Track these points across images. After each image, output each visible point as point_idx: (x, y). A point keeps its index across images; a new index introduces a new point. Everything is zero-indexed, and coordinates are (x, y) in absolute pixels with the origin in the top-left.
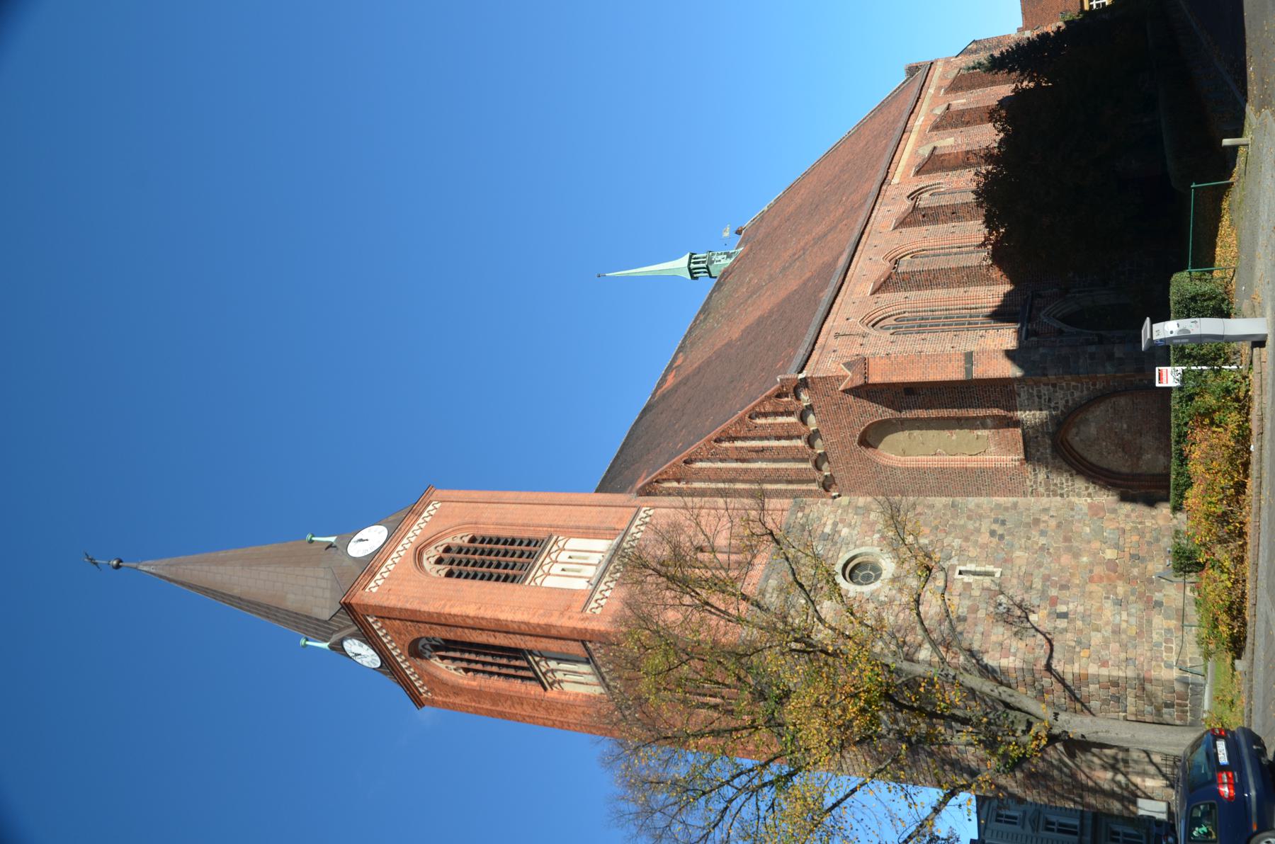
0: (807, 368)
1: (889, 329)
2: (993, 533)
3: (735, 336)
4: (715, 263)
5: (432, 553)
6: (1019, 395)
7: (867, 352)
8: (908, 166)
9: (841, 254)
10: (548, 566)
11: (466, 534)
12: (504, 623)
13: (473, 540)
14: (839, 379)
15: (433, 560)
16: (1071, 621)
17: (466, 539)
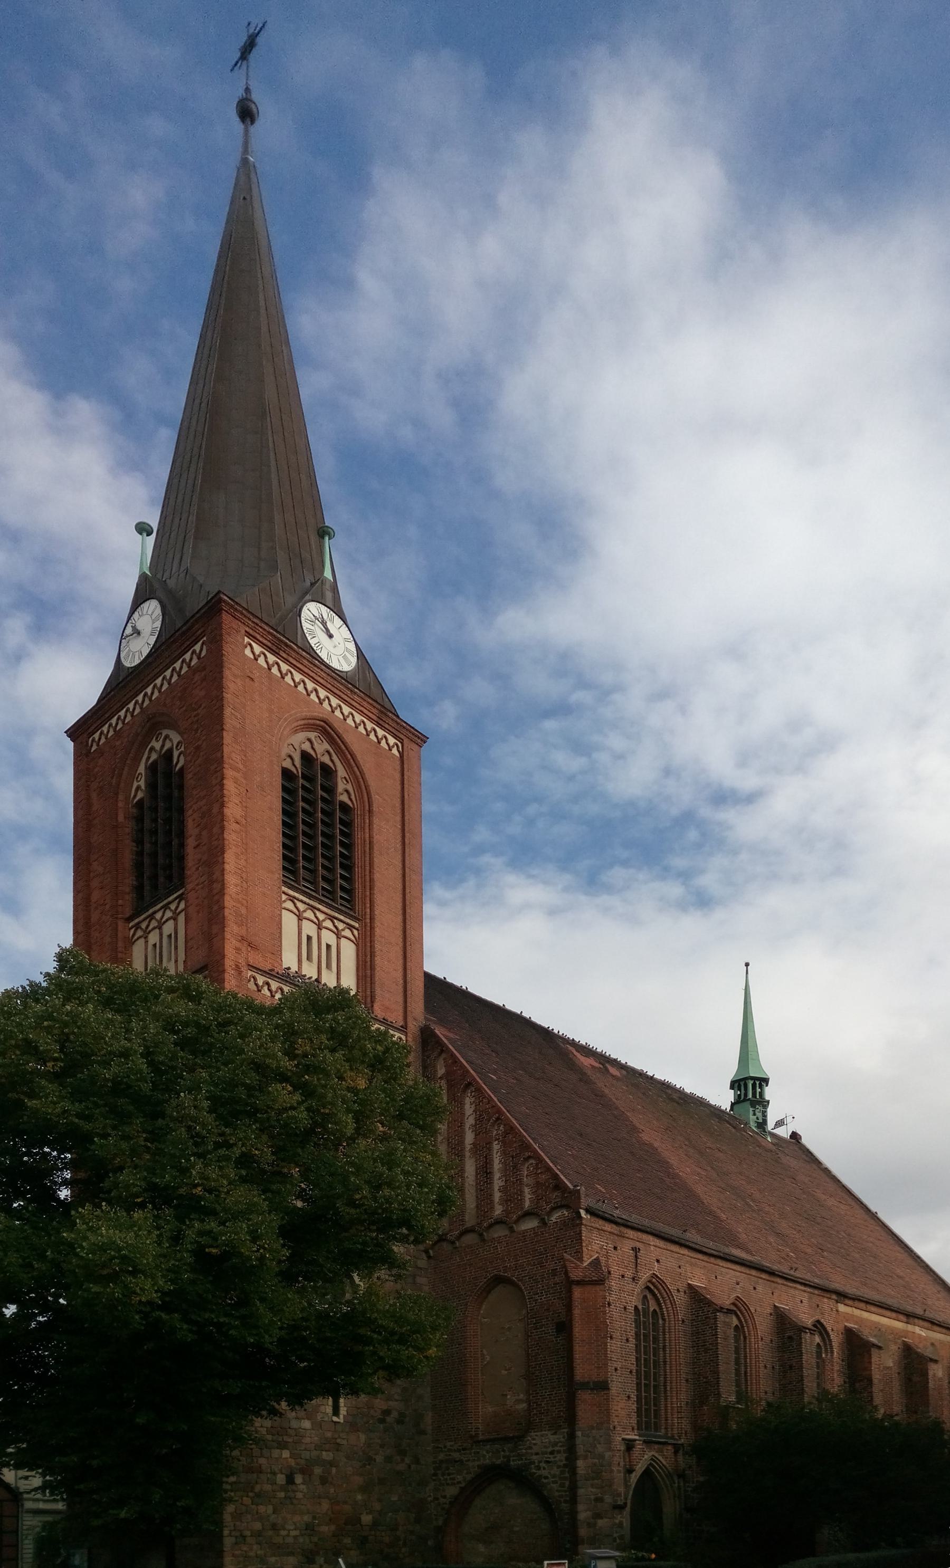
0: (594, 1219)
1: (643, 1304)
2: (387, 1412)
3: (645, 1137)
4: (751, 1109)
5: (321, 748)
6: (555, 1434)
7: (614, 1283)
8: (860, 1321)
9: (748, 1251)
10: (312, 917)
11: (353, 797)
12: (220, 859)
13: (344, 808)
14: (579, 1255)
15: (307, 747)
16: (282, 1488)
17: (344, 798)
